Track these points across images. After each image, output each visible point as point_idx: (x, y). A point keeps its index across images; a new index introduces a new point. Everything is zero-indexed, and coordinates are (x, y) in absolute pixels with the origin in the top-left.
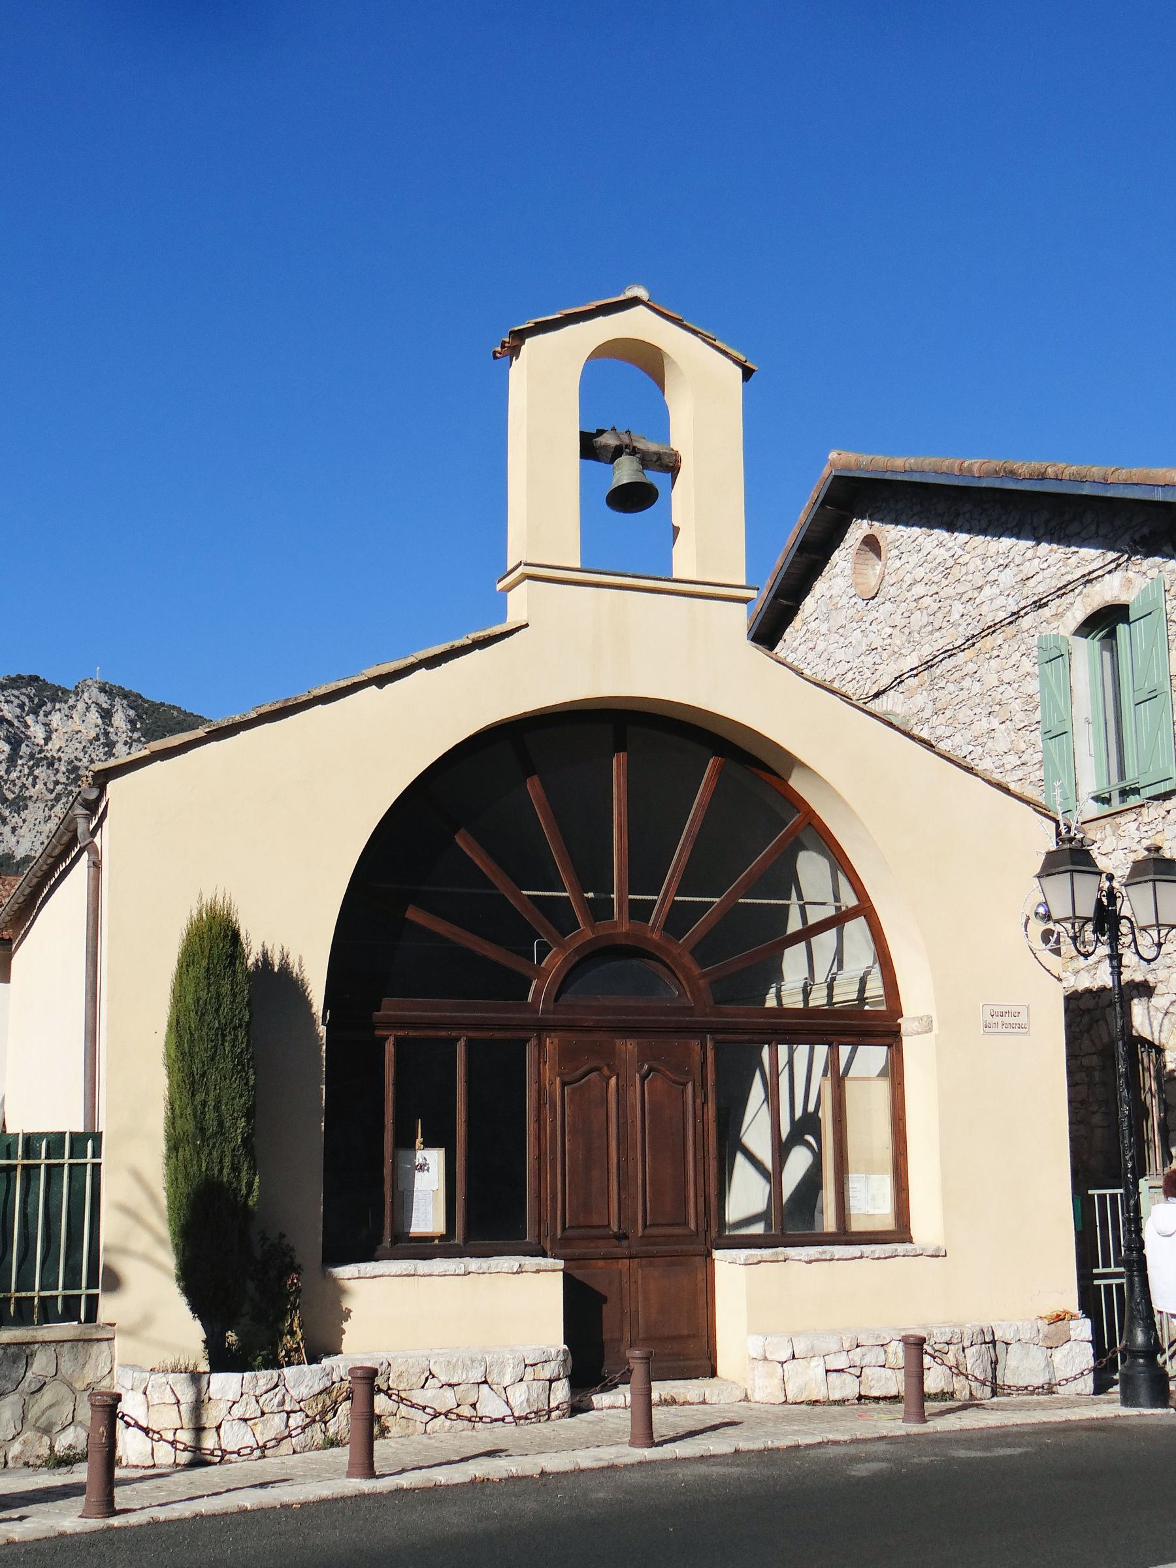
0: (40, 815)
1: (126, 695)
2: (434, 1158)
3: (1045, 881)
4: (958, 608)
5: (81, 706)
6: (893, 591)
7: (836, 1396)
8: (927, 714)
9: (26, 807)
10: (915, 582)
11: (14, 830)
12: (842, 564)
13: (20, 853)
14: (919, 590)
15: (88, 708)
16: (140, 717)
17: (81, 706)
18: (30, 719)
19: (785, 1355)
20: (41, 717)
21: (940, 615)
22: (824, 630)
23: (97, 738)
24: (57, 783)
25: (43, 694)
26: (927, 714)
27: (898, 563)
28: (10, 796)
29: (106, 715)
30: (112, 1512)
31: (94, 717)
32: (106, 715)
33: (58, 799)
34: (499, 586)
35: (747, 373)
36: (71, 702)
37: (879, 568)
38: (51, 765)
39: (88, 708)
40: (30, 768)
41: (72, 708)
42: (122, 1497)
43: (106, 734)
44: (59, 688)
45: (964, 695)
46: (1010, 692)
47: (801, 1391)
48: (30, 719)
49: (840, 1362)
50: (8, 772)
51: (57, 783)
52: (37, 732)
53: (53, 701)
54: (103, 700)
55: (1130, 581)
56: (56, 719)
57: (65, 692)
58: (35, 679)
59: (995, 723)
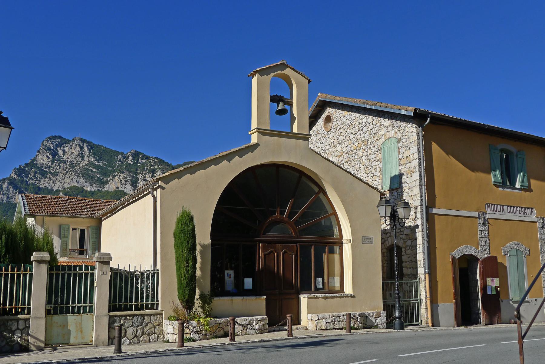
0: (61, 177)
1: (88, 142)
2: (231, 272)
3: (379, 208)
4: (352, 136)
5: (74, 145)
6: (334, 130)
7: (329, 328)
8: (343, 162)
9: (58, 175)
10: (340, 128)
11: (53, 182)
12: (320, 122)
13: (55, 189)
14: (341, 130)
15: (76, 145)
16: (92, 148)
17: (74, 145)
18: (59, 149)
19: (317, 319)
20: (62, 148)
21: (347, 137)
22: (315, 139)
23: (79, 155)
24: (67, 168)
25: (62, 141)
26: (343, 162)
27: (336, 123)
28: (52, 172)
29: (82, 148)
30: (184, 347)
31: (78, 148)
32: (82, 148)
33: (67, 173)
34: (249, 133)
35: (309, 82)
36: (71, 144)
37: (330, 124)
38: (65, 163)
39: (76, 145)
40: (59, 164)
41: (71, 146)
42: (185, 344)
43: (82, 153)
44: (68, 140)
45: (353, 158)
46: (365, 158)
47: (320, 327)
48: (59, 149)
49: (329, 320)
50: (52, 164)
51: (67, 168)
52: (60, 152)
53: (66, 143)
54: (81, 144)
55: (396, 132)
56: (66, 149)
57: (70, 141)
58: (60, 137)
59: (361, 166)
